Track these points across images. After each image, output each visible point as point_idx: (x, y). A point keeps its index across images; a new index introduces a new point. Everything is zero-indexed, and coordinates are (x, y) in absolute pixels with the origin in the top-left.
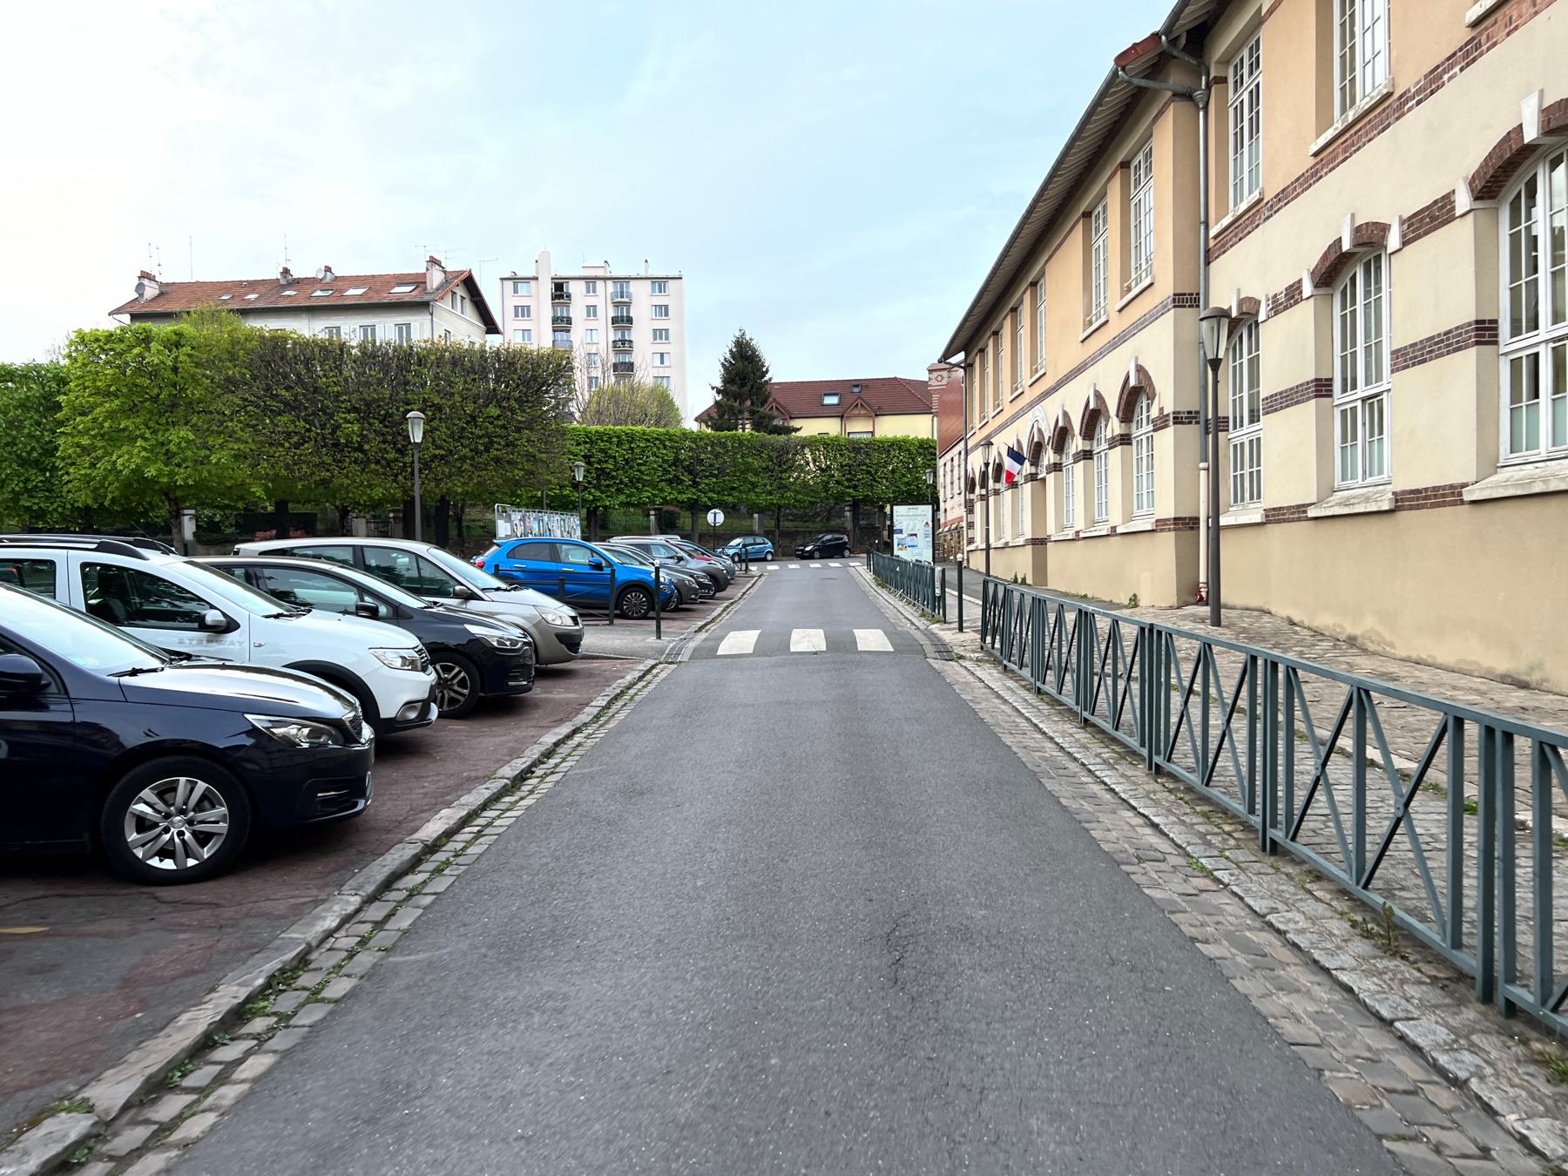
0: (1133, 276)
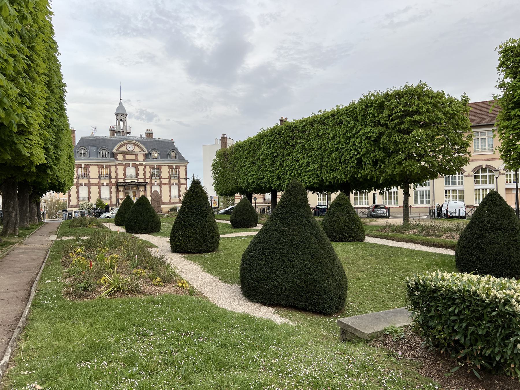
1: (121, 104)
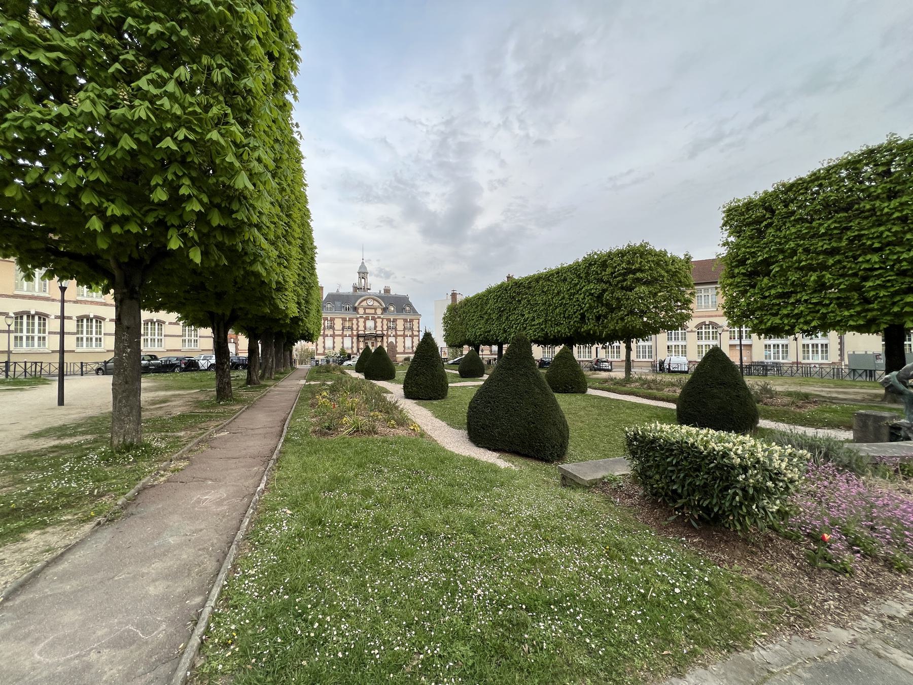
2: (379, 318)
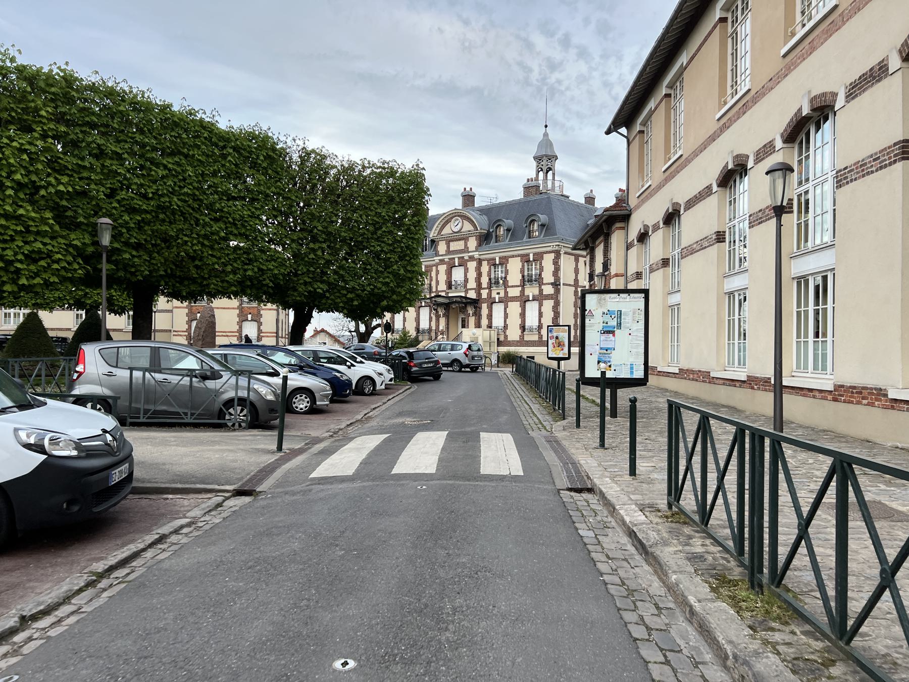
0: (672, 152)
1: (546, 135)
2: (472, 258)
